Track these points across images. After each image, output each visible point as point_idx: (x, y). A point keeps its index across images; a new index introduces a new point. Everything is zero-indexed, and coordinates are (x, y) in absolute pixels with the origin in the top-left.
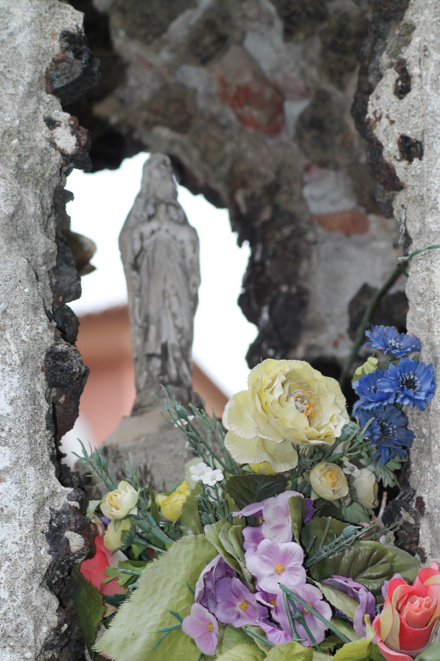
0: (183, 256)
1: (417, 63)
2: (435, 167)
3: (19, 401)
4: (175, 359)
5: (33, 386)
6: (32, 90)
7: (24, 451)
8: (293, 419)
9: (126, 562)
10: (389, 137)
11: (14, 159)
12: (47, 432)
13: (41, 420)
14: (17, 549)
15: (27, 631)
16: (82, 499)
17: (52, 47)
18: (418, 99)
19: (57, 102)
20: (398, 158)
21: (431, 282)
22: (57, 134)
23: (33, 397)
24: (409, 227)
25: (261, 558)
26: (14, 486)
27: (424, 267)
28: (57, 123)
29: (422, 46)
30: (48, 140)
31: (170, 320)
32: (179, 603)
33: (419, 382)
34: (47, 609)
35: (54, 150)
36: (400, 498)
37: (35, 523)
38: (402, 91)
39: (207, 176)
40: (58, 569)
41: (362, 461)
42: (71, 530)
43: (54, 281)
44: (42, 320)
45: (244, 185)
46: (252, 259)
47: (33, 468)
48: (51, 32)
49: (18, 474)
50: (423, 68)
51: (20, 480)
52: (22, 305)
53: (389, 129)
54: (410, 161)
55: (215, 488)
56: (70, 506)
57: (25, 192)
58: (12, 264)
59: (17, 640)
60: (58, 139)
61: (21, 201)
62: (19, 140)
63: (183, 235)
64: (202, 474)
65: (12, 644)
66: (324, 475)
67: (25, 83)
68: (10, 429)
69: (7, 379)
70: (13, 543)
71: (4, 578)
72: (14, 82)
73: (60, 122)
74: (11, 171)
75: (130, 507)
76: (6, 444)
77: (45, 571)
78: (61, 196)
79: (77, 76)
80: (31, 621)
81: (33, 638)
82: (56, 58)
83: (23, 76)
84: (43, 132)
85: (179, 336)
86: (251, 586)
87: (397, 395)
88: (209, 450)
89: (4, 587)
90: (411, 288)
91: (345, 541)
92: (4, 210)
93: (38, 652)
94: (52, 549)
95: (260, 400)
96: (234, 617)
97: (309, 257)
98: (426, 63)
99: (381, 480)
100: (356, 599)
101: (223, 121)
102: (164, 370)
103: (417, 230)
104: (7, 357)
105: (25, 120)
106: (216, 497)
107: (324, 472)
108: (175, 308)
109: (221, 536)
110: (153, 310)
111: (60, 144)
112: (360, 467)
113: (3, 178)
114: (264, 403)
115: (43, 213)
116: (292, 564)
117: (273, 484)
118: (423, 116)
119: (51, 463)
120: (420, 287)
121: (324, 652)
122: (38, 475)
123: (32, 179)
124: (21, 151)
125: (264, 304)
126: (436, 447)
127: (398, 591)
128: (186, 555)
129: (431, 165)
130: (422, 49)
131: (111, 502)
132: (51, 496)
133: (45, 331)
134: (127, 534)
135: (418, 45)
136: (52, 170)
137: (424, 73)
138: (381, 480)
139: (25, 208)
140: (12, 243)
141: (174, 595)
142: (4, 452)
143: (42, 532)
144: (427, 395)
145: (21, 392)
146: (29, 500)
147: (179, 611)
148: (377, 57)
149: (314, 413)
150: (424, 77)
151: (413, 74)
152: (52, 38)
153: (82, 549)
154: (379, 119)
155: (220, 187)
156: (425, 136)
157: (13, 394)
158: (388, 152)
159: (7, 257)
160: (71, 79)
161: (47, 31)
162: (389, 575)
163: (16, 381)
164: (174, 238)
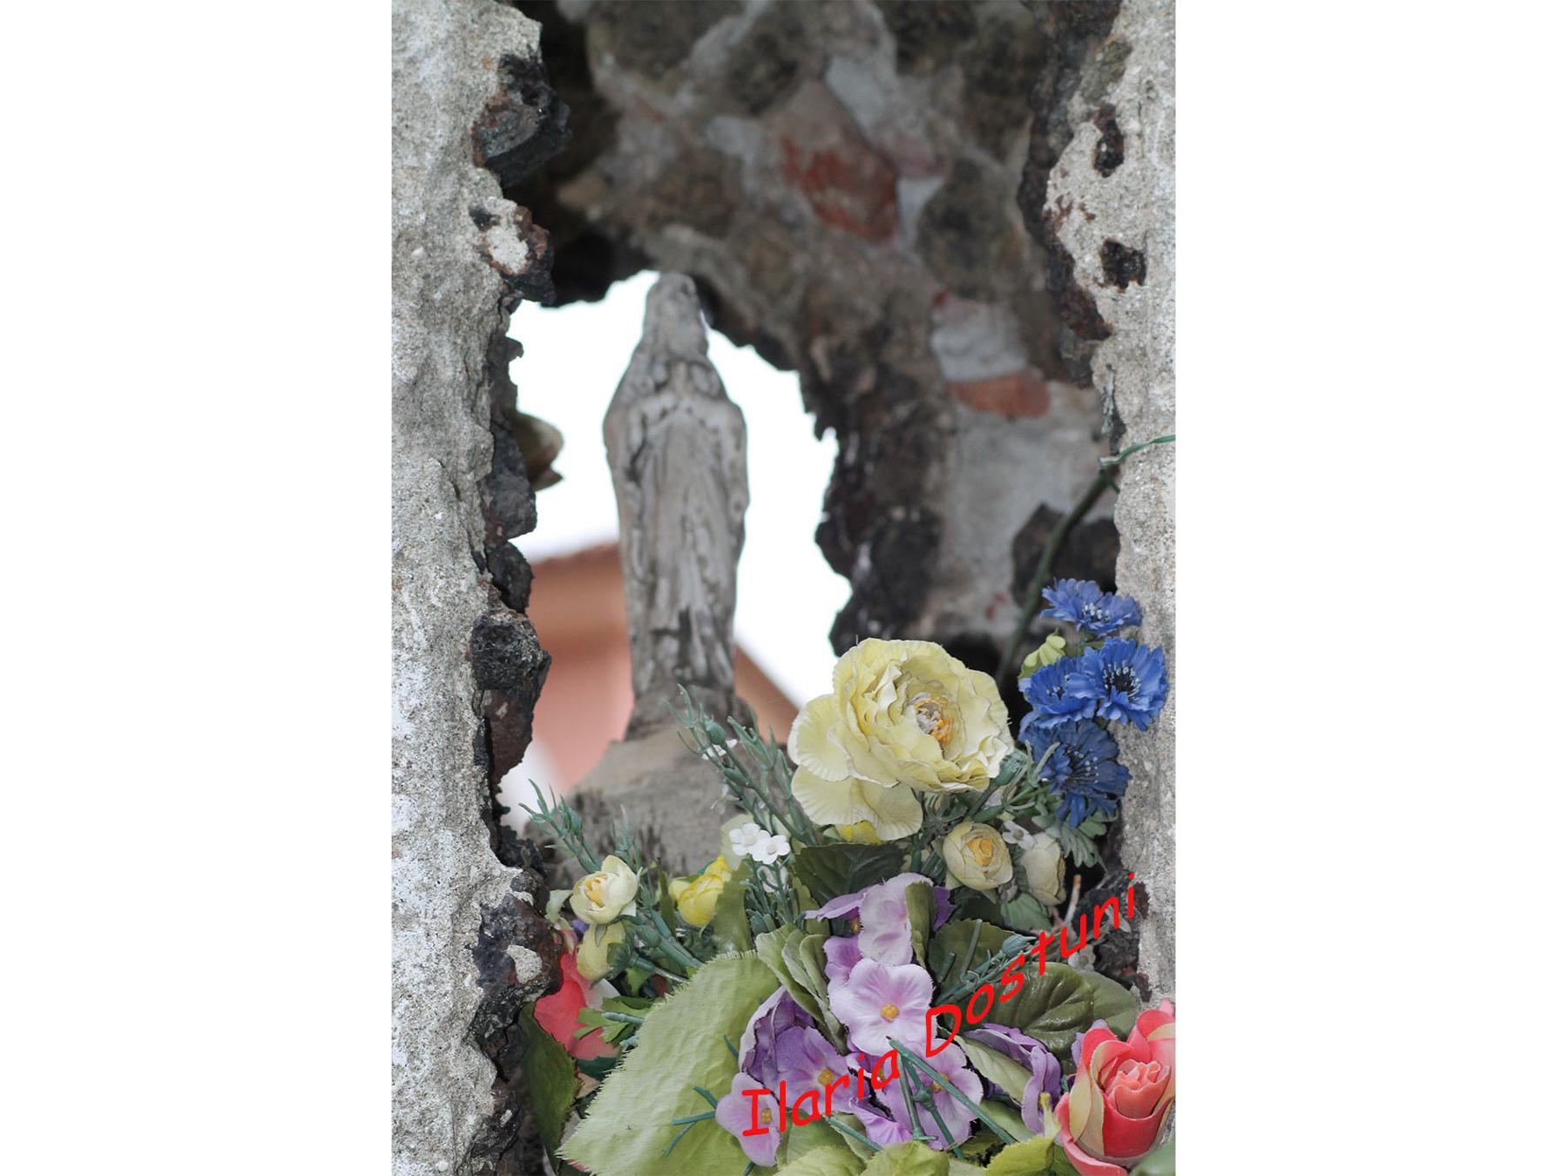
0: (718, 456)
1: (1135, 112)
4: (703, 639)
8: (914, 746)
9: (616, 999)
11: (416, 282)
12: (476, 769)
19: (492, 182)
20: (1101, 281)
23: (450, 707)
24: (1119, 404)
31: (695, 568)
38: (1108, 161)
39: (760, 313)
40: (494, 1013)
41: (1036, 820)
43: (488, 499)
45: (827, 329)
46: (840, 460)
49: (423, 844)
54: (1123, 286)
55: (774, 868)
61: (428, 357)
62: (426, 248)
63: (718, 418)
64: (752, 843)
66: (969, 845)
67: (437, 148)
68: (410, 763)
72: (416, 146)
78: (500, 349)
79: (528, 135)
81: (450, 1135)
82: (492, 104)
84: (469, 236)
85: (711, 598)
86: (839, 1042)
87: (1099, 703)
88: (765, 800)
95: (856, 712)
97: (942, 458)
100: (1025, 1065)
101: (789, 216)
102: (684, 659)
103: (1135, 410)
104: (403, 634)
108: (703, 548)
110: (663, 553)
111: (498, 256)
112: (1034, 830)
117: (878, 862)
118: (1146, 206)
121: (970, 1159)
123: (448, 318)
124: (430, 269)
125: (862, 541)
127: (1100, 1052)
130: (1144, 87)
132: (483, 882)
133: (471, 588)
135: (1136, 81)
137: (1148, 131)
142: (399, 803)
144: (1152, 704)
145: (429, 698)
146: (443, 889)
147: (711, 1086)
148: (1064, 102)
153: (538, 977)
154: (1067, 211)
155: (783, 333)
156: (1149, 241)
157: (414, 701)
158: (1084, 270)
160: (518, 141)
162: (1084, 1022)
163: (421, 677)
164: (702, 423)
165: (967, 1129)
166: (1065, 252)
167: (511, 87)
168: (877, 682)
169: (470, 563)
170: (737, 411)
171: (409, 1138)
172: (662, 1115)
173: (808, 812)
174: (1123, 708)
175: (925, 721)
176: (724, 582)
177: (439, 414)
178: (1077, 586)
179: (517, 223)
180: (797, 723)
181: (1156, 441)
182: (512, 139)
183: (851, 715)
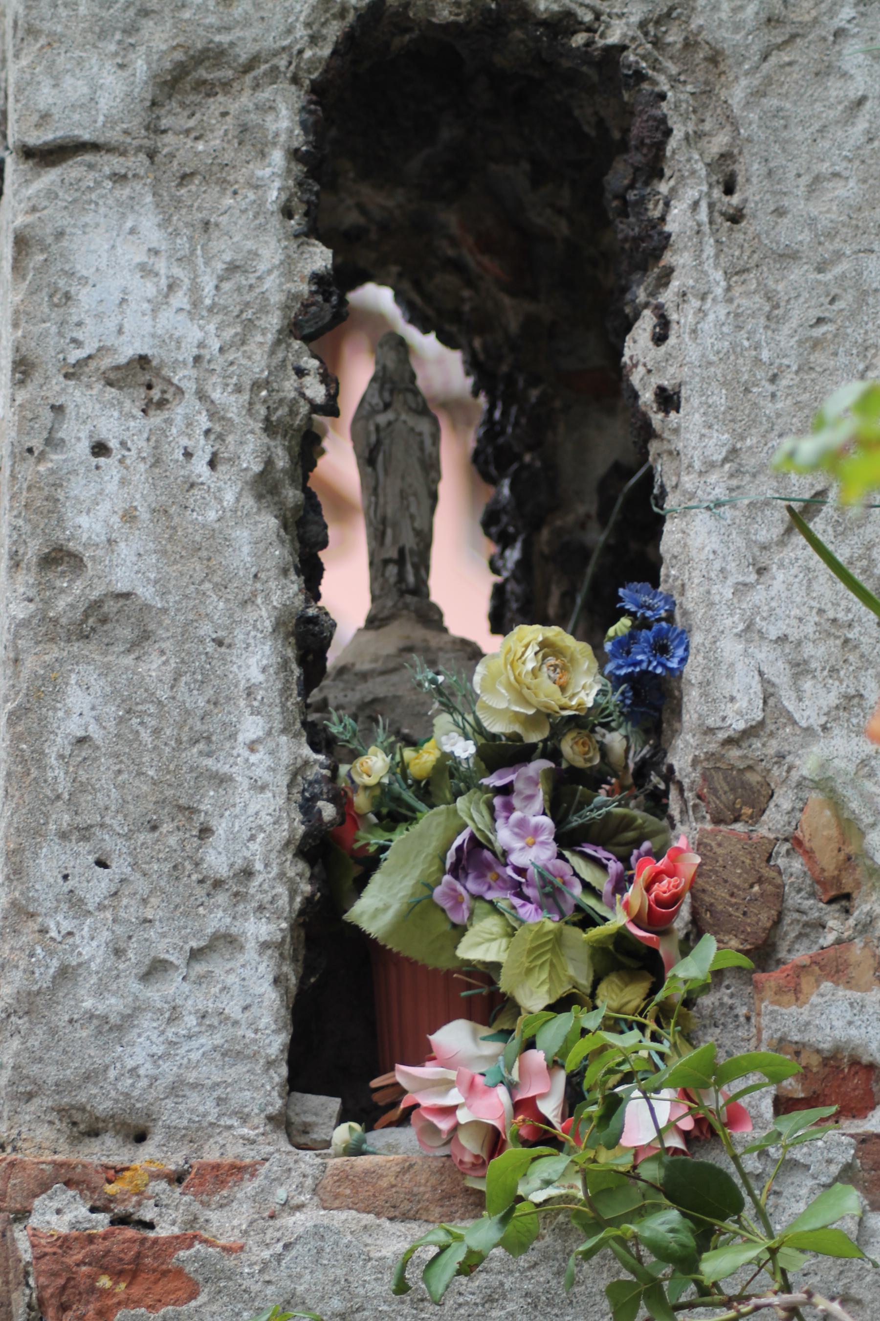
0: (422, 448)
8: (548, 693)
9: (376, 825)
11: (263, 411)
21: (685, 545)
23: (284, 665)
26: (266, 757)
30: (296, 389)
31: (408, 522)
38: (660, 339)
49: (271, 744)
54: (667, 412)
64: (454, 745)
69: (259, 646)
76: (259, 713)
87: (650, 662)
100: (604, 868)
102: (401, 577)
111: (309, 393)
116: (543, 838)
124: (270, 403)
125: (505, 477)
128: (439, 824)
133: (296, 595)
146: (282, 770)
149: (567, 683)
154: (635, 366)
157: (265, 662)
162: (637, 843)
168: (523, 654)
169: (294, 577)
173: (485, 724)
174: (664, 666)
176: (426, 529)
180: (479, 669)
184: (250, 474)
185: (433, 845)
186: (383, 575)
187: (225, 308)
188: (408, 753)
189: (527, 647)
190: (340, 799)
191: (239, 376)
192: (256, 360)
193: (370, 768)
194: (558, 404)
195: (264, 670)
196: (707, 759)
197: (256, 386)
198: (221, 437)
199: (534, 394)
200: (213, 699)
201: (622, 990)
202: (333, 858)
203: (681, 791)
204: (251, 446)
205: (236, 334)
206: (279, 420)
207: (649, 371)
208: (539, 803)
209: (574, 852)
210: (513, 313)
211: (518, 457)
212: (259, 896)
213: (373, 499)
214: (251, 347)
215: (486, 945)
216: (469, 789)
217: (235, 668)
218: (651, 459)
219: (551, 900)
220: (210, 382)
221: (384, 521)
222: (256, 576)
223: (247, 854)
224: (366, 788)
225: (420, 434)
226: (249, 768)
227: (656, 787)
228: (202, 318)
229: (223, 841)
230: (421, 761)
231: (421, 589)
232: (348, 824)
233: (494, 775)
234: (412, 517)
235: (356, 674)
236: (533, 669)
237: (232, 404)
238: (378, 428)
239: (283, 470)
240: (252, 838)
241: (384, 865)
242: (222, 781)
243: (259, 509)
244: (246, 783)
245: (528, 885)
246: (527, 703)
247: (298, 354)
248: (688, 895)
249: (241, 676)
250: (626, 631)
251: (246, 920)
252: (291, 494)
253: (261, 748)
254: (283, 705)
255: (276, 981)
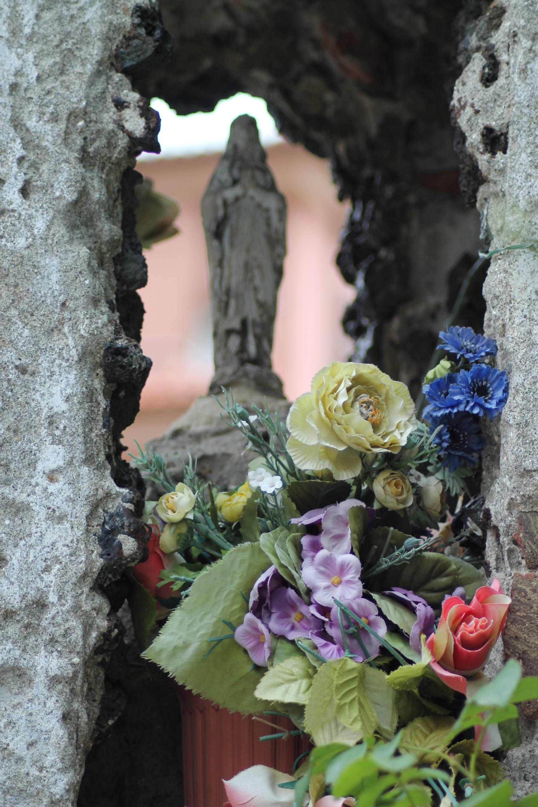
0: (268, 223)
1: (506, 49)
2: (519, 163)
3: (75, 398)
5: (90, 383)
6: (101, 68)
7: (78, 451)
8: (358, 428)
9: (182, 565)
10: (473, 128)
11: (79, 142)
12: (103, 431)
13: (98, 418)
14: (68, 552)
15: (76, 636)
16: (138, 501)
17: (123, 23)
18: (505, 89)
19: (126, 81)
20: (481, 150)
21: (507, 284)
22: (125, 115)
23: (90, 395)
24: (490, 223)
25: (317, 569)
27: (502, 268)
28: (125, 104)
29: (512, 31)
30: (115, 122)
32: (231, 612)
33: (491, 389)
34: (97, 614)
35: (122, 133)
36: (470, 506)
37: (88, 526)
38: (489, 79)
40: (110, 573)
41: (430, 468)
42: (124, 534)
44: (102, 313)
47: (87, 469)
48: (123, 7)
49: (71, 475)
50: (511, 55)
51: (73, 481)
52: (82, 298)
53: (473, 119)
54: (494, 154)
56: (124, 507)
57: (90, 177)
58: (73, 254)
59: (65, 645)
60: (126, 121)
61: (84, 187)
62: (85, 121)
63: (271, 202)
64: (262, 480)
65: (59, 649)
66: (389, 483)
67: (94, 62)
68: (65, 427)
69: (64, 375)
70: (64, 546)
71: (54, 581)
72: (82, 60)
73: (130, 103)
74: (76, 155)
75: (186, 511)
76: (60, 442)
77: (96, 575)
79: (149, 53)
80: (80, 626)
81: (81, 643)
82: (127, 35)
83: (92, 53)
84: (111, 114)
86: (306, 598)
87: (468, 402)
88: (272, 453)
89: (53, 591)
90: (487, 289)
91: (406, 554)
92: (66, 196)
93: (87, 657)
94: (104, 552)
95: (324, 405)
96: (288, 628)
98: (515, 50)
99: (449, 488)
102: (243, 348)
103: (499, 227)
104: (64, 351)
105: (92, 100)
106: (274, 504)
107: (389, 480)
109: (278, 545)
111: (128, 126)
112: (427, 473)
113: (68, 162)
114: (327, 408)
115: (110, 197)
116: (348, 577)
117: (336, 492)
118: (509, 106)
119: (107, 463)
120: (497, 289)
121: (379, 667)
122: (92, 476)
123: (97, 163)
124: (87, 134)
126: (505, 458)
127: (453, 610)
128: (242, 562)
129: (514, 159)
130: (511, 35)
131: (167, 504)
132: (105, 498)
133: (105, 325)
134: (184, 537)
135: (507, 30)
136: (119, 153)
137: (512, 61)
138: (449, 488)
139: (89, 193)
140: (75, 231)
141: (227, 604)
142: (58, 451)
143: (95, 535)
144: (498, 404)
145: (78, 389)
146: (81, 501)
147: (233, 619)
148: (468, 37)
150: (511, 65)
151: (502, 61)
152: (124, 13)
153: (135, 553)
154: (463, 107)
156: (510, 128)
157: (69, 391)
158: (472, 143)
159: (68, 247)
160: (142, 57)
161: (119, 5)
162: (450, 589)
163: (73, 377)
165: (378, 650)
166: (461, 131)
167: (139, 25)
169: (105, 308)
170: (282, 199)
171: (58, 644)
172: (203, 635)
173: (295, 462)
174: (481, 406)
175: (364, 411)
176: (270, 301)
177: (91, 219)
178: (460, 330)
179: (139, 107)
181: (508, 248)
182: (139, 56)
183: (321, 407)
184: (63, 202)
185: (236, 582)
186: (226, 345)
187: (45, 37)
188: (221, 498)
189: (339, 383)
190: (145, 535)
191: (56, 105)
192: (75, 90)
193: (175, 504)
194: (412, 199)
195: (67, 399)
196: (524, 503)
197: (73, 116)
198: (35, 166)
199: (389, 191)
200: (13, 427)
201: (426, 736)
202: (131, 589)
203: (498, 536)
204: (66, 175)
205: (55, 63)
206: (97, 151)
207: (477, 112)
208: (347, 543)
209: (384, 596)
210: (372, 112)
211: (375, 251)
212: (51, 629)
213: (218, 271)
214: (70, 77)
215: (286, 686)
216: (275, 526)
217: (37, 396)
218: (478, 205)
219: (355, 642)
220: (26, 110)
221: (228, 292)
222: (63, 304)
223: (41, 585)
224: (172, 524)
225: (267, 210)
226: (47, 498)
227: (473, 535)
228: (21, 46)
229: (16, 571)
230: (232, 504)
231: (262, 359)
232: (152, 562)
233: (305, 516)
234: (256, 290)
235: (191, 436)
236: (344, 404)
237: (48, 133)
238: (225, 204)
239: (99, 202)
240: (47, 569)
241: (185, 602)
242: (18, 511)
243: (71, 240)
244: (43, 513)
245: (331, 626)
246: (340, 441)
247: (119, 86)
248: (499, 644)
249: (43, 404)
250: (445, 373)
251: (36, 653)
252: (107, 227)
253: (61, 478)
254: (86, 436)
255: (65, 717)
